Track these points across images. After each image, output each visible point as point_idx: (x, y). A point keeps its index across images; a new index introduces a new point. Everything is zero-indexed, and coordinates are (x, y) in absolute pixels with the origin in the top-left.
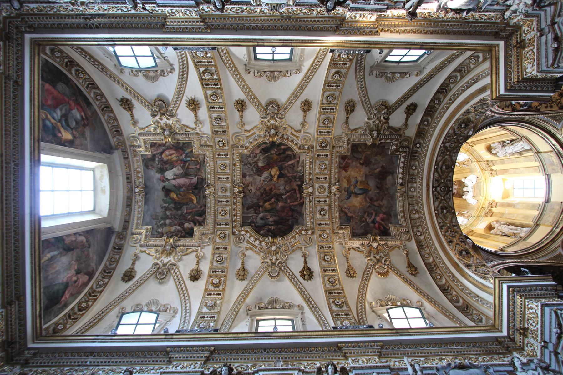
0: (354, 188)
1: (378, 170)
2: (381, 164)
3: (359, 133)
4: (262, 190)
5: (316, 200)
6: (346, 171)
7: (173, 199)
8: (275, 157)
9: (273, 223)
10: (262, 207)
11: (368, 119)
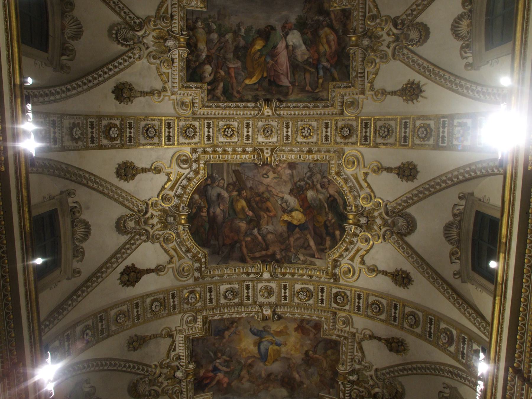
0: (269, 341)
1: (297, 376)
2: (307, 382)
3: (356, 354)
4: (266, 195)
6: (296, 330)
7: (252, 44)
8: (322, 219)
9: (212, 214)
10: (239, 195)
11: (377, 370)
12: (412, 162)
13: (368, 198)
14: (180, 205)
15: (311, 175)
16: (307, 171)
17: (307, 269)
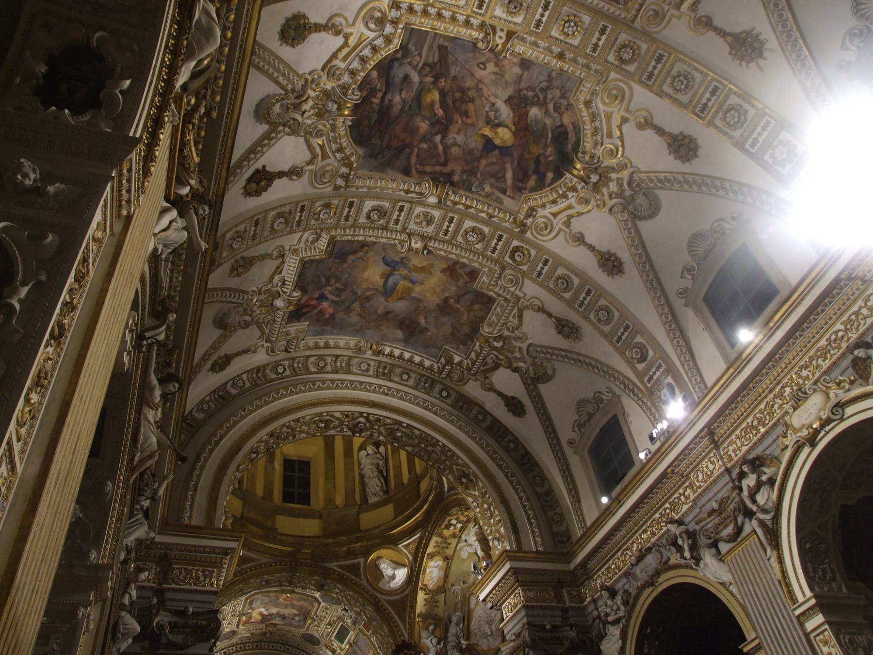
0: (401, 275)
2: (433, 330)
5: (407, 205)
6: (443, 271)
8: (536, 150)
9: (386, 102)
10: (435, 83)
12: (696, 139)
13: (613, 153)
14: (350, 86)
15: (547, 87)
16: (544, 79)
17: (489, 205)
